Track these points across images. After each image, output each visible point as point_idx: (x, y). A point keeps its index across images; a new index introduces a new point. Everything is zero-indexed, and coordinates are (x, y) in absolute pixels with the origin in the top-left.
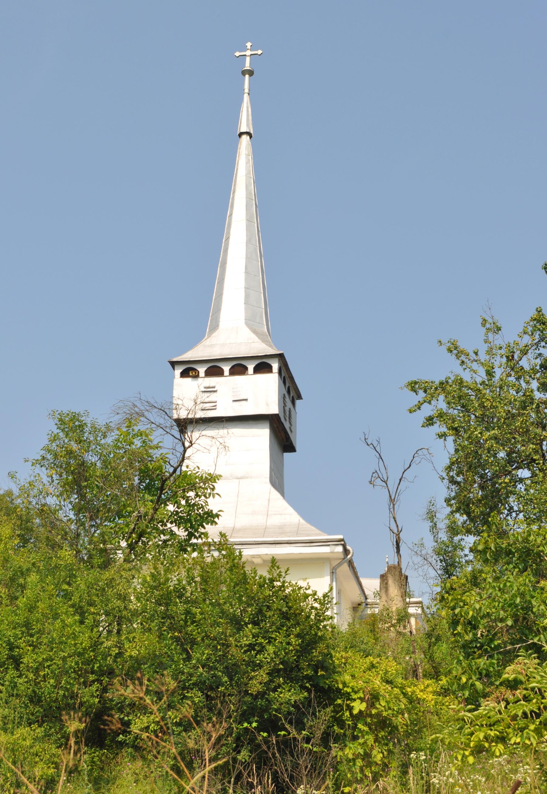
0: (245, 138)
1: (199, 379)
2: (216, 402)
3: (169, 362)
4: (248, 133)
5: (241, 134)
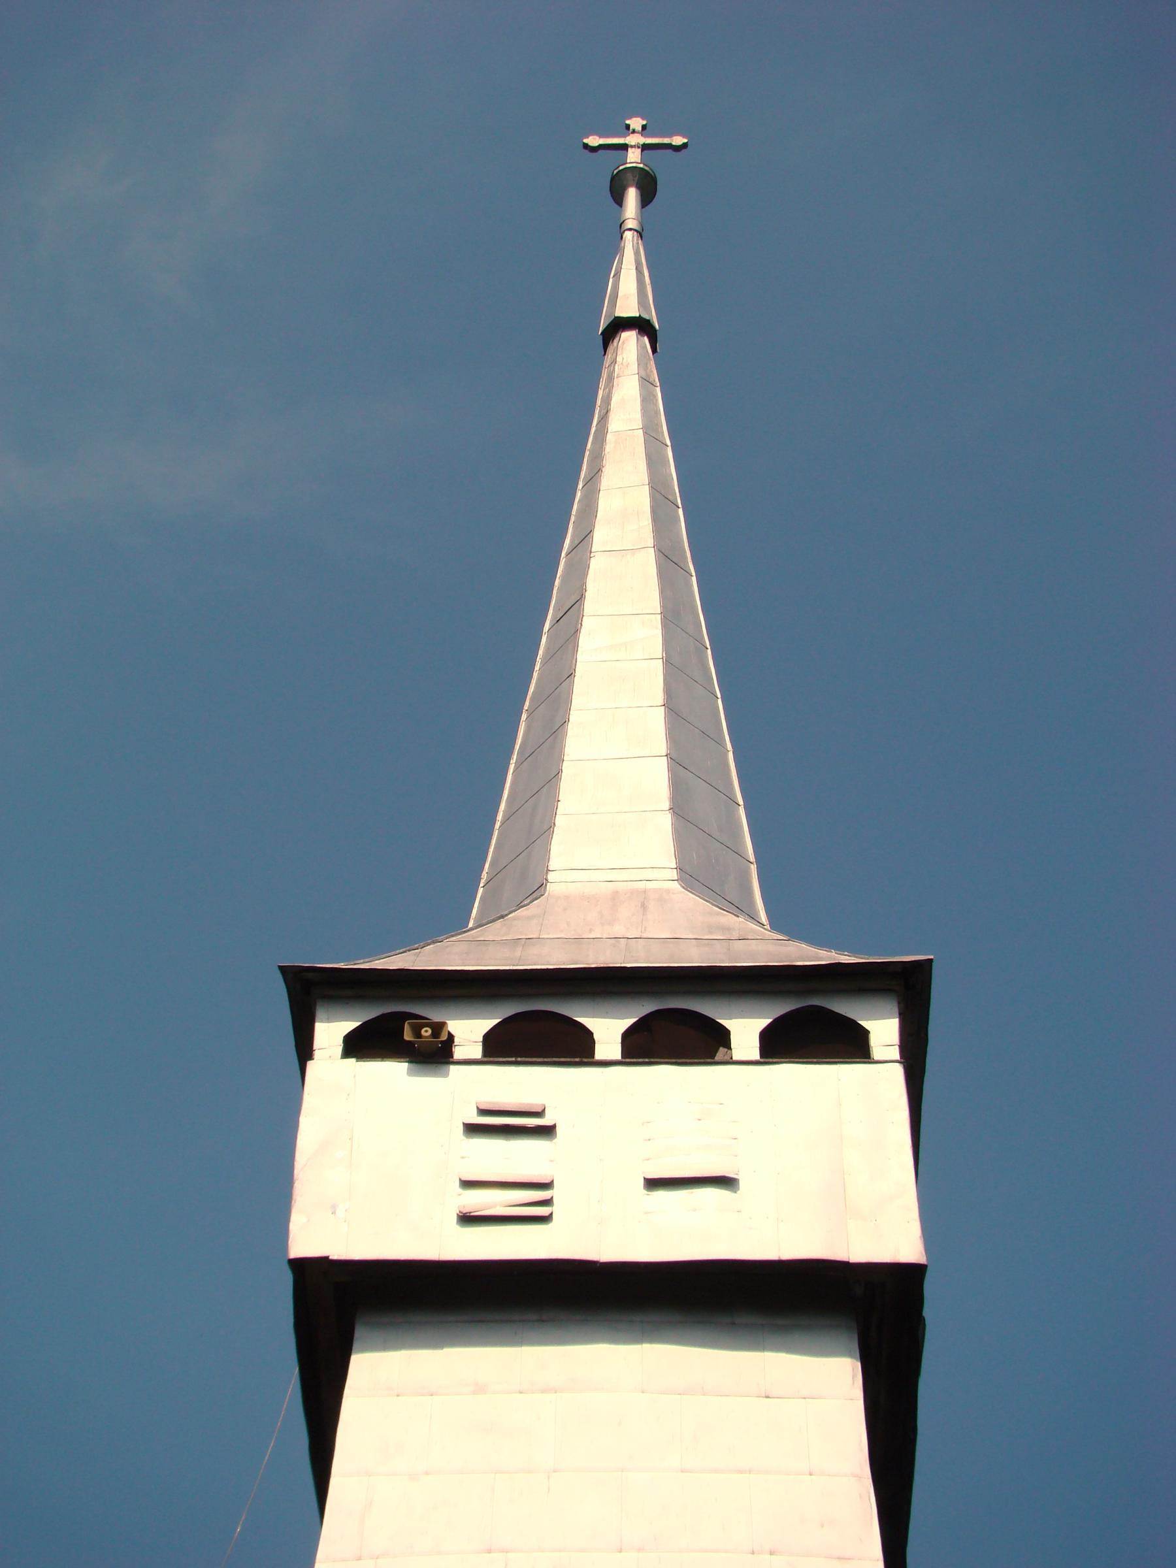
0: (630, 343)
1: (453, 1068)
2: (547, 1186)
3: (283, 969)
4: (640, 325)
5: (619, 325)
